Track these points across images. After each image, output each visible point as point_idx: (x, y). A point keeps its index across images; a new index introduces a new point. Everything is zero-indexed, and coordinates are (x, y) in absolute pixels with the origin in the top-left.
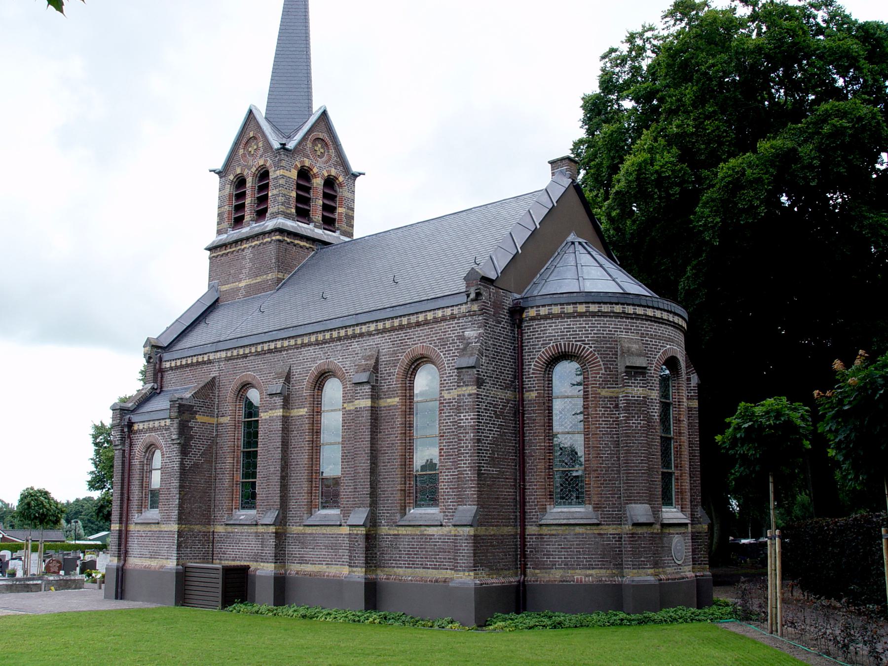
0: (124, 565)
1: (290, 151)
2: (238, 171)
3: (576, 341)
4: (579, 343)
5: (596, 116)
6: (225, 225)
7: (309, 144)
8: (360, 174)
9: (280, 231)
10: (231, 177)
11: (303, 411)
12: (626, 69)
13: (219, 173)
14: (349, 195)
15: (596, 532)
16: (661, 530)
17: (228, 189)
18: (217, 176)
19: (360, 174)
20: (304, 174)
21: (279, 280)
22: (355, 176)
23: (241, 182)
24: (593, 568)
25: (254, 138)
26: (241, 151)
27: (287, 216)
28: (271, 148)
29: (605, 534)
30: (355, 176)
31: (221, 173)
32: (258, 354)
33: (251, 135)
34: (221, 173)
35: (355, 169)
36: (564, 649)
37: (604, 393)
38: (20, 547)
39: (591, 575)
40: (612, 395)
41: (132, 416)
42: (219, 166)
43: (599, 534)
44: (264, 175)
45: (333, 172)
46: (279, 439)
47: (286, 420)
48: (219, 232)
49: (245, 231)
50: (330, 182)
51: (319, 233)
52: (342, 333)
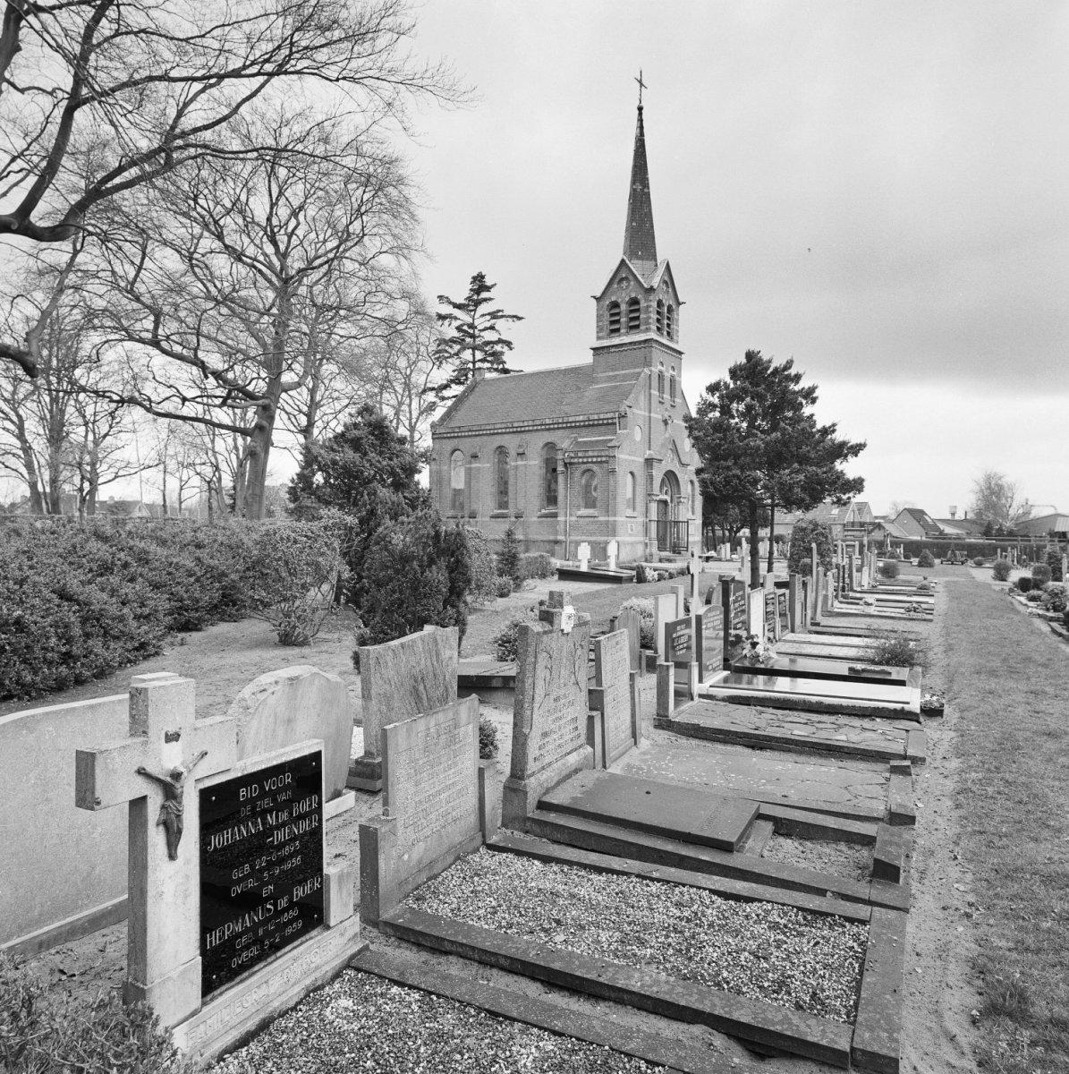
13: (598, 299)
20: (660, 304)
23: (615, 305)
26: (616, 286)
35: (681, 300)
42: (598, 294)
44: (634, 302)
51: (665, 341)
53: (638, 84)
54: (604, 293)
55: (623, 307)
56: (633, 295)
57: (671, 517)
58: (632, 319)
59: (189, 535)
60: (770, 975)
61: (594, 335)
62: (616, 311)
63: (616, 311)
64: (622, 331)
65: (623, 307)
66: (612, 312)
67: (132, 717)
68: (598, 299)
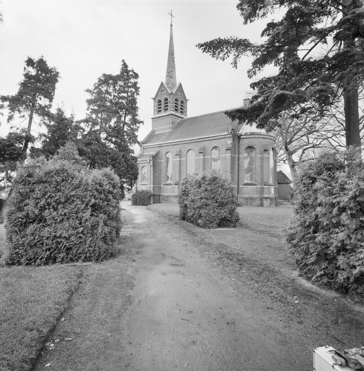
0: (118, 213)
2: (159, 99)
5: (186, 188)
6: (156, 112)
9: (172, 114)
10: (157, 100)
11: (184, 159)
12: (90, 334)
13: (154, 99)
17: (156, 103)
18: (153, 100)
23: (160, 101)
25: (163, 90)
26: (160, 94)
27: (173, 111)
28: (168, 93)
32: (171, 145)
33: (162, 89)
35: (187, 99)
37: (330, 271)
41: (109, 171)
42: (154, 97)
44: (166, 99)
46: (179, 165)
47: (180, 161)
48: (154, 114)
51: (179, 115)
52: (191, 141)
53: (170, 16)
54: (156, 96)
55: (162, 102)
56: (166, 97)
57: (20, 198)
58: (166, 106)
59: (98, 181)
60: (298, 354)
61: (153, 113)
62: (167, 102)
63: (167, 102)
64: (162, 111)
65: (179, 102)
66: (165, 102)
67: (51, 260)
68: (154, 99)
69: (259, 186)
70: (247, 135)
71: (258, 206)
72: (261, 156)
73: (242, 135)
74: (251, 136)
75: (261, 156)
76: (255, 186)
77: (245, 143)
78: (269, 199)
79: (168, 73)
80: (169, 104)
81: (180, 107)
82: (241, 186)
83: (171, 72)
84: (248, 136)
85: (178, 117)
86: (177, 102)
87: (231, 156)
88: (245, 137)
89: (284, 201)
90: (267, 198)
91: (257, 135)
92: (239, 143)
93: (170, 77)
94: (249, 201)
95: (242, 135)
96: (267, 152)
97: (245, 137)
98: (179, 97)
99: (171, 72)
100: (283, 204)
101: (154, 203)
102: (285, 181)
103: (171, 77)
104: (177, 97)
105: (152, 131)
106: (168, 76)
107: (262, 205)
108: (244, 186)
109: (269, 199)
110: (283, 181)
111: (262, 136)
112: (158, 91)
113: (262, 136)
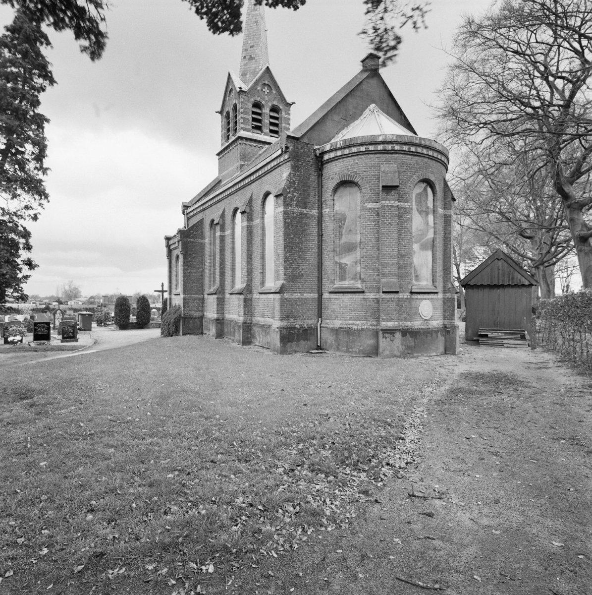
1: (245, 92)
3: (351, 173)
4: (352, 174)
7: (259, 88)
8: (293, 103)
14: (287, 116)
15: (362, 297)
16: (411, 296)
19: (293, 103)
20: (257, 105)
21: (242, 166)
22: (289, 105)
24: (360, 320)
29: (367, 298)
30: (289, 105)
31: (221, 113)
34: (221, 113)
35: (289, 101)
36: (140, 473)
38: (143, 302)
39: (358, 325)
40: (375, 207)
42: (219, 110)
43: (364, 298)
45: (275, 103)
49: (230, 141)
50: (274, 109)
65: (266, 110)
69: (372, 296)
70: (337, 149)
71: (369, 355)
72: (377, 205)
73: (326, 152)
74: (347, 151)
75: (377, 205)
76: (361, 296)
77: (334, 172)
78: (398, 335)
79: (246, 50)
80: (250, 117)
81: (266, 121)
82: (326, 295)
83: (252, 47)
84: (339, 153)
85: (259, 142)
86: (260, 109)
87: (285, 212)
88: (332, 155)
89: (507, 336)
90: (390, 332)
91: (362, 144)
92: (320, 175)
93: (249, 60)
94: (343, 338)
95: (326, 152)
96: (393, 192)
97: (332, 155)
98: (264, 99)
99: (252, 47)
100: (502, 345)
101: (184, 334)
102: (513, 278)
103: (251, 58)
104: (258, 99)
105: (217, 178)
106: (245, 57)
107: (374, 352)
108: (333, 296)
109: (398, 335)
110: (506, 279)
111: (380, 147)
112: (225, 94)
113: (380, 147)
